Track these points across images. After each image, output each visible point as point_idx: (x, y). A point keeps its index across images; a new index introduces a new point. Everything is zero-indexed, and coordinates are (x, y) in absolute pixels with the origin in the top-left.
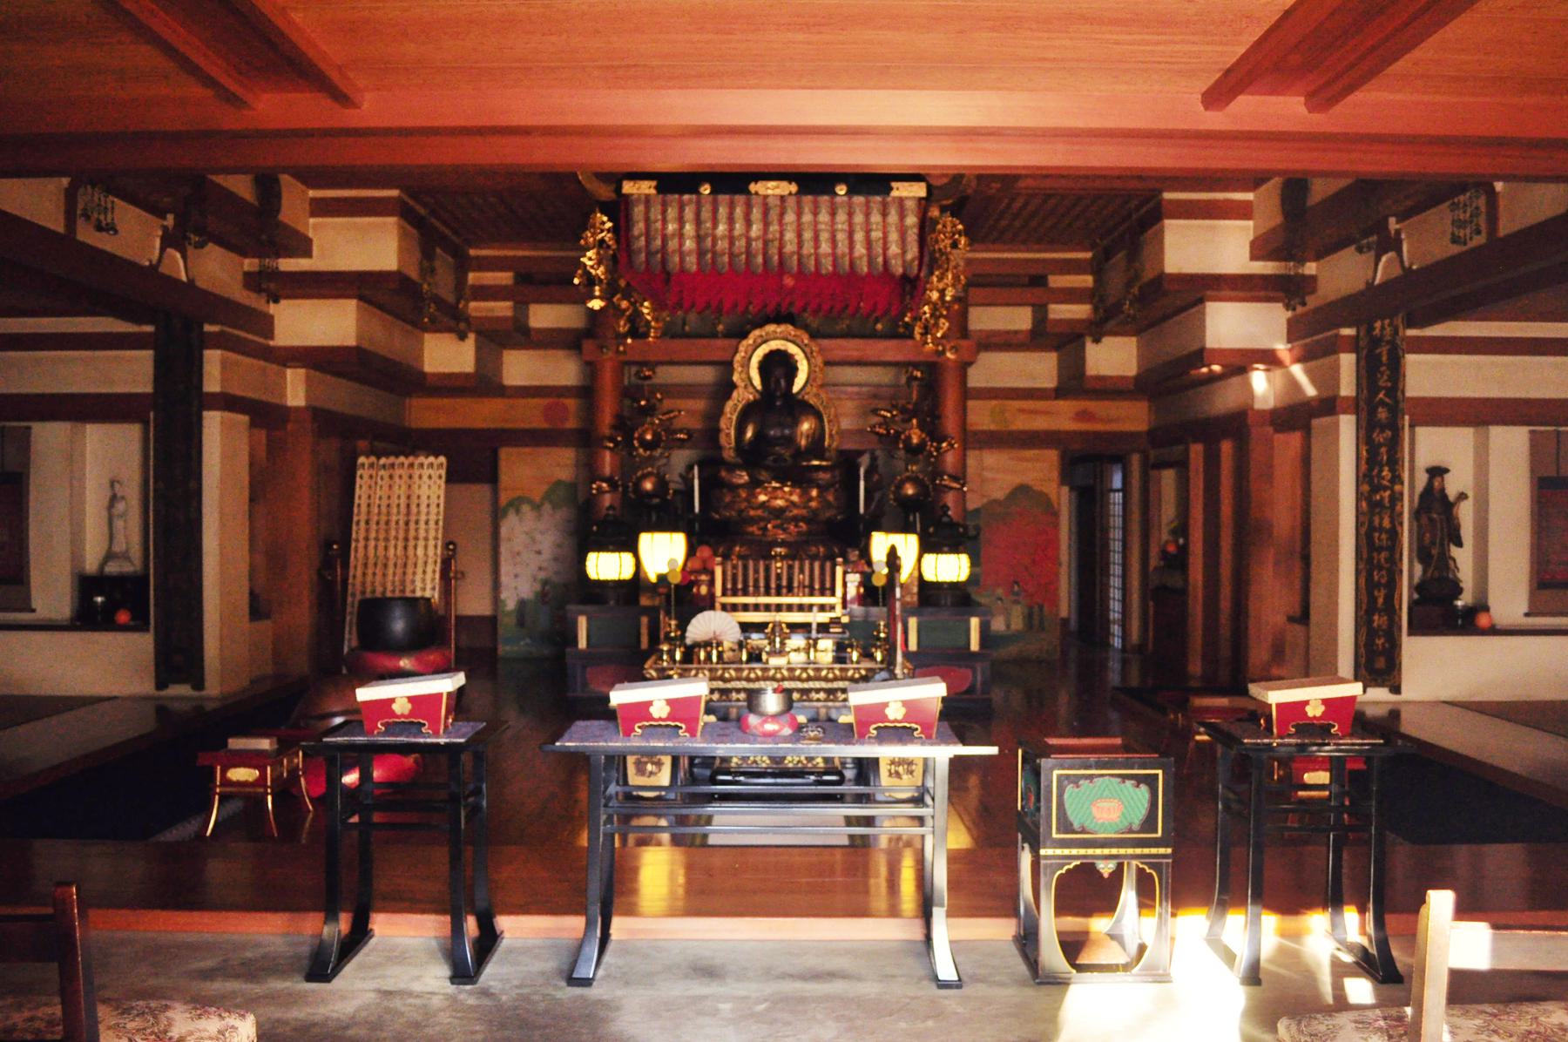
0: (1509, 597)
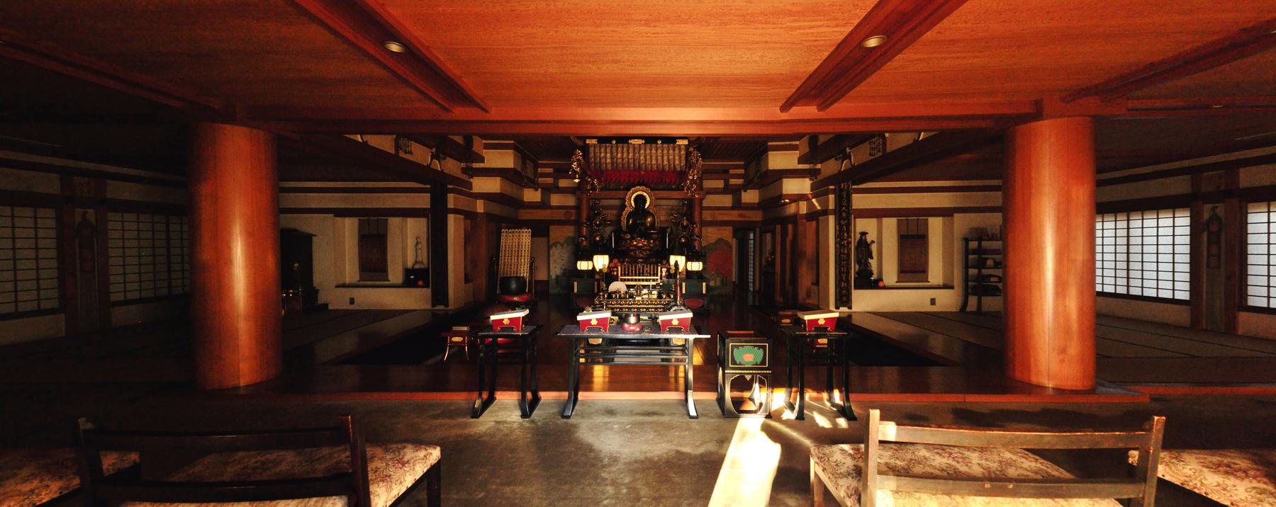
0: (890, 276)
